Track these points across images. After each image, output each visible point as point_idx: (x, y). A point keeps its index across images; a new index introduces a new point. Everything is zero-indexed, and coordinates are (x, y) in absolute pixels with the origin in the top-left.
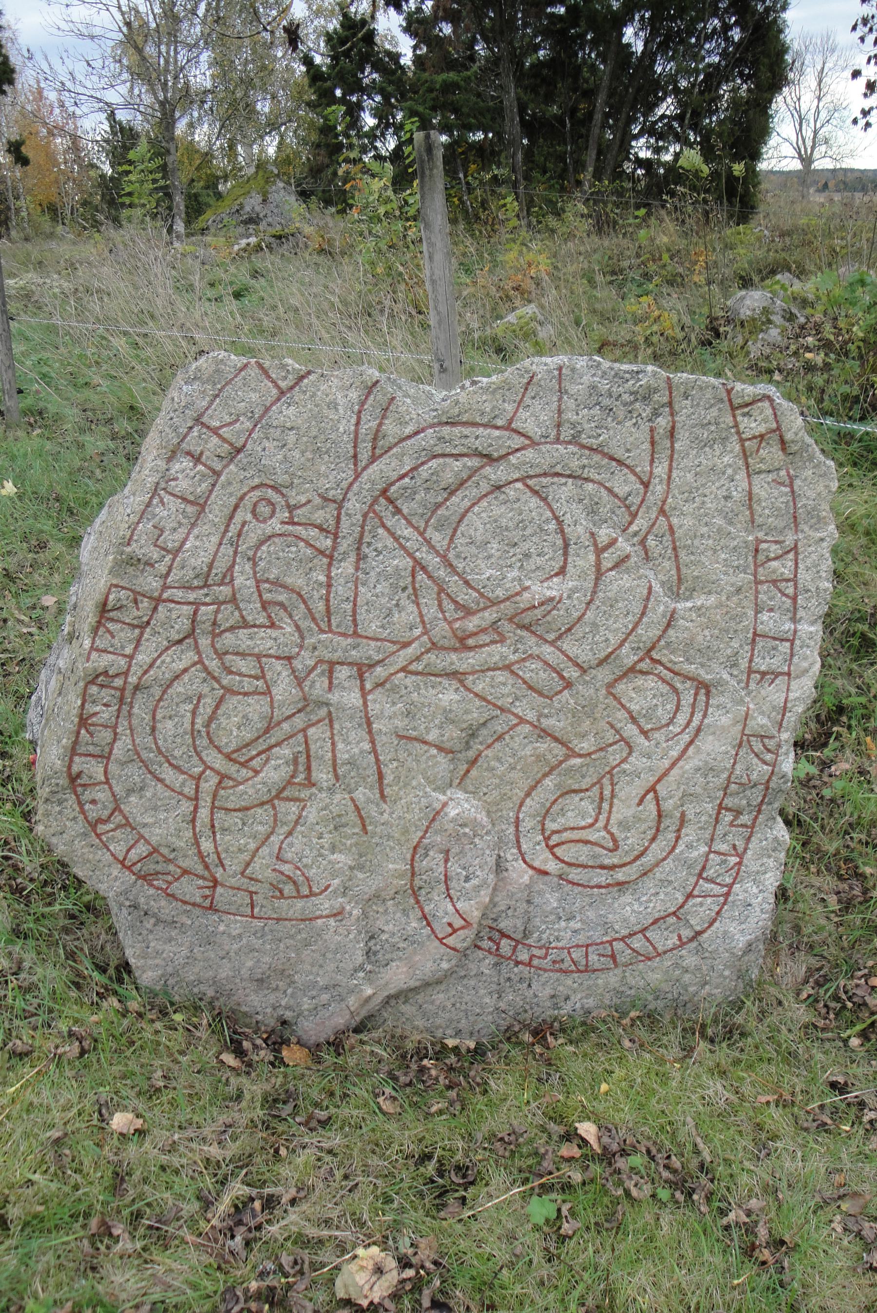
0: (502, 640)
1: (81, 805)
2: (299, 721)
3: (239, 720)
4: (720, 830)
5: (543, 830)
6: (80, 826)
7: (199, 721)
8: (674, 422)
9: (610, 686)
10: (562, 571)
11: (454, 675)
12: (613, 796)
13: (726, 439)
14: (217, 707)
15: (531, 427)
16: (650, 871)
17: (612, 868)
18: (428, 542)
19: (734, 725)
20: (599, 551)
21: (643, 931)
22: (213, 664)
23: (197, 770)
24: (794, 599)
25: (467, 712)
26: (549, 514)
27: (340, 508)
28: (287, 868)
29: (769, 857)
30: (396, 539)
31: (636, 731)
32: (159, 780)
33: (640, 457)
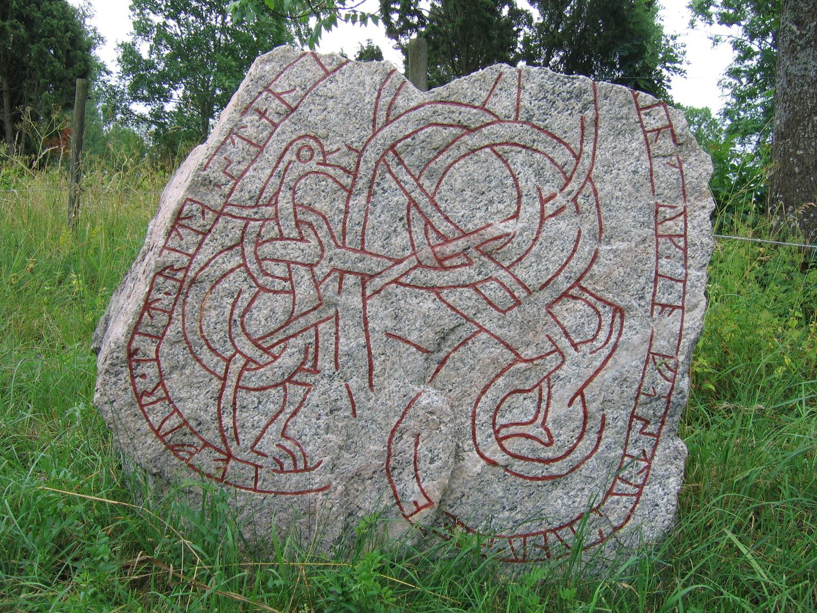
0: (470, 263)
1: (133, 377)
2: (312, 318)
3: (266, 313)
4: (634, 435)
5: (494, 424)
6: (129, 396)
7: (236, 312)
8: (597, 115)
9: (549, 306)
10: (516, 216)
12: (549, 397)
13: (633, 130)
16: (578, 467)
17: (548, 461)
18: (420, 186)
20: (543, 202)
22: (253, 267)
24: (685, 250)
25: (441, 318)
26: (508, 172)
28: (288, 444)
29: (672, 464)
30: (398, 183)
31: (568, 344)
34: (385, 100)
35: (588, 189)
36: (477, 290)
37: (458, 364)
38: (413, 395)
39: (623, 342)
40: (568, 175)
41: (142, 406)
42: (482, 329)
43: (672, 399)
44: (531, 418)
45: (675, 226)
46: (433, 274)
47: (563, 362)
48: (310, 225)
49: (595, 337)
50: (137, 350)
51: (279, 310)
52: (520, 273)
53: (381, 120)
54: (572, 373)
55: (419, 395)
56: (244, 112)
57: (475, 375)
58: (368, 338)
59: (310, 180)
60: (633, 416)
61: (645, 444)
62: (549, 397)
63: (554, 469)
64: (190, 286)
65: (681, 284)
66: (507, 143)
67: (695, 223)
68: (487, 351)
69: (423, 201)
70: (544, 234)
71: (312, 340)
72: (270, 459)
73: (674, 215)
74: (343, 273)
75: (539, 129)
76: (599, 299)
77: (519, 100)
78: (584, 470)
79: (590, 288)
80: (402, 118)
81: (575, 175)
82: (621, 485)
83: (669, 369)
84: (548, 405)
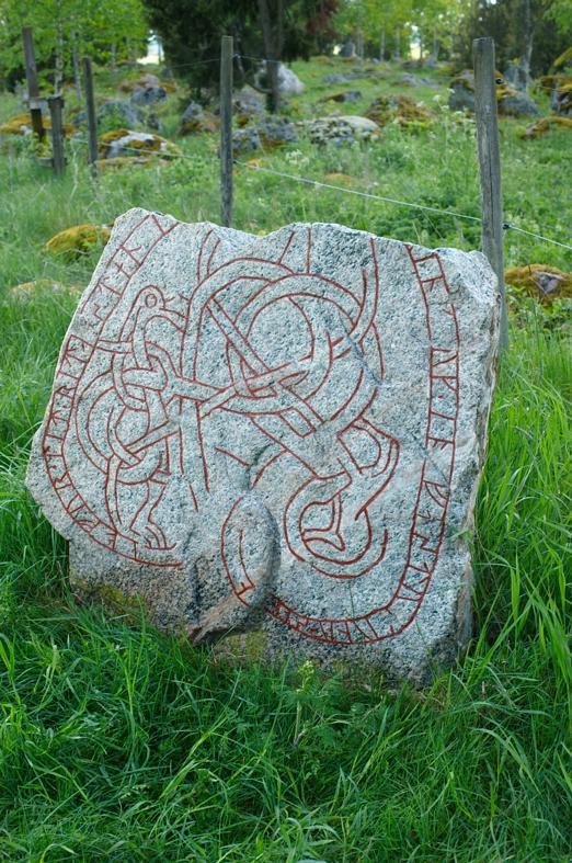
0: (275, 395)
1: (48, 468)
2: (163, 431)
3: (132, 424)
4: (415, 550)
5: (300, 528)
6: (46, 482)
7: (112, 424)
8: (377, 267)
9: (340, 434)
10: (311, 356)
11: (247, 414)
12: (341, 511)
13: (411, 280)
14: (122, 415)
15: (291, 265)
16: (367, 570)
17: (343, 563)
18: (237, 329)
19: (416, 472)
20: (331, 345)
21: (367, 617)
22: (120, 390)
23: (108, 455)
24: (457, 391)
25: (254, 439)
26: (303, 318)
27: (189, 304)
28: (152, 527)
29: (450, 578)
30: (219, 326)
31: (354, 467)
32: (89, 458)
33: (357, 288)
34: (205, 257)
35: (371, 334)
36: (281, 417)
37: (271, 476)
38: (236, 499)
39: (399, 470)
40: (354, 321)
41: (56, 489)
42: (287, 450)
43: (446, 522)
44: (328, 526)
45: (447, 369)
46: (247, 402)
47: (351, 483)
48: (157, 358)
49: (376, 464)
50: (49, 447)
51: (139, 425)
52: (315, 404)
53: (203, 273)
54: (357, 492)
55: (241, 499)
56: (108, 265)
57: (284, 486)
58: (202, 450)
59: (155, 322)
60: (412, 533)
61: (426, 557)
62: (341, 511)
63: (349, 570)
64: (79, 402)
65: (453, 422)
66: (301, 294)
67: (465, 366)
68: (291, 468)
69: (238, 342)
70: (332, 373)
71: (164, 449)
72: (142, 538)
73: (446, 359)
74: (182, 398)
75: (327, 280)
76: (379, 431)
77: (309, 256)
78: (373, 574)
79: (371, 421)
80: (219, 272)
81: (360, 321)
82: (404, 590)
83: (442, 496)
84: (340, 516)
